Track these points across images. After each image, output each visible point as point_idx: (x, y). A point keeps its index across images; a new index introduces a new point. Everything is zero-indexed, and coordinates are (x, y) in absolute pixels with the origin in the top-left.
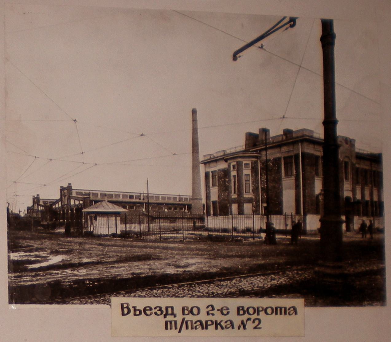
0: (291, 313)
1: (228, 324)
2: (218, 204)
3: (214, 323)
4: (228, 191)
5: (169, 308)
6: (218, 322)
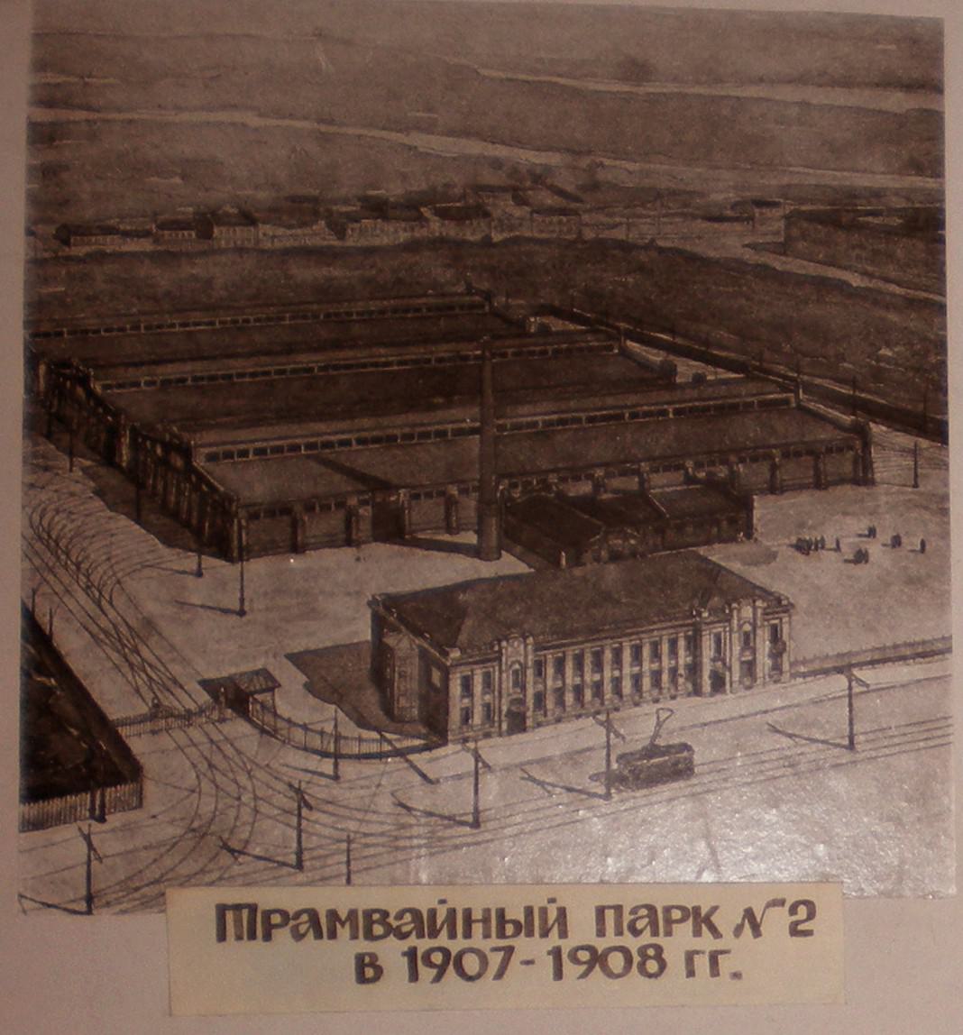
0: (303, 929)
1: (406, 924)
2: (662, 336)
3: (422, 958)
4: (482, 436)
5: (606, 911)
6: (704, 912)
